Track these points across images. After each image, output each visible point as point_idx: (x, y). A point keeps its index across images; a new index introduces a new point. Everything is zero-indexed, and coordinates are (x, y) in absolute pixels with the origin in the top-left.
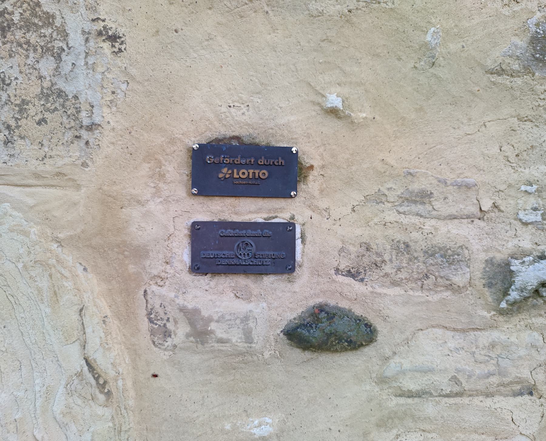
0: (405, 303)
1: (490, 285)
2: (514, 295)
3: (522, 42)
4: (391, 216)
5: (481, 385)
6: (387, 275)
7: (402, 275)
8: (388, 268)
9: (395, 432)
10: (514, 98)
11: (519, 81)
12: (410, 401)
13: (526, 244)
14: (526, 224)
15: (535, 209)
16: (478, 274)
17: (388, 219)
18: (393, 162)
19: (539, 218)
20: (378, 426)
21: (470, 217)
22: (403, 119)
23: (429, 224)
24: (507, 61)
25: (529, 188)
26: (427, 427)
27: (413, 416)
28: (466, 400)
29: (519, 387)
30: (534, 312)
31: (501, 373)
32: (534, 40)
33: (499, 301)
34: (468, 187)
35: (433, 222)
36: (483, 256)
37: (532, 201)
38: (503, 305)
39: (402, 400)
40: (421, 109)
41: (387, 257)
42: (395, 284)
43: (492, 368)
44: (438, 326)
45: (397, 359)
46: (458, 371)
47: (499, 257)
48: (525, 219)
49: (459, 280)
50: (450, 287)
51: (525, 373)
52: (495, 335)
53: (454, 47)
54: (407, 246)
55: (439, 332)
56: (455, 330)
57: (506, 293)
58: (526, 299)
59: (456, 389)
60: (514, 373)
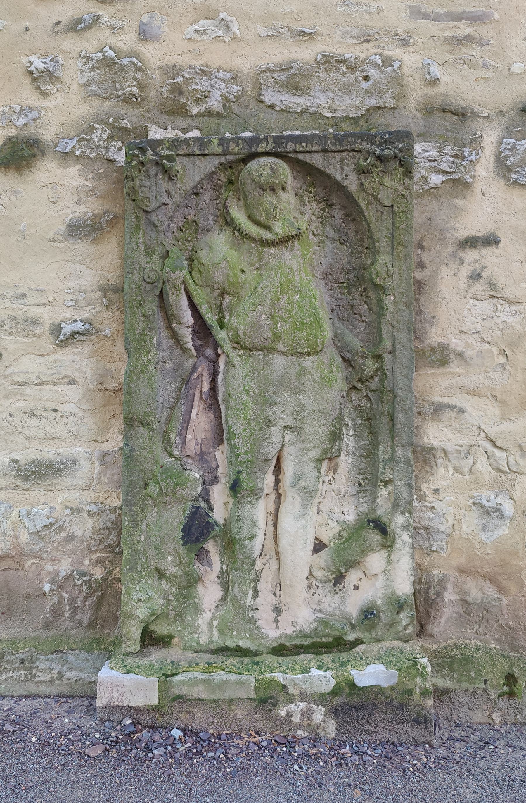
0: (15, 343)
1: (52, 334)
2: (61, 337)
3: (63, 228)
4: (8, 305)
5: (50, 379)
6: (6, 330)
7: (13, 330)
8: (6, 327)
9: (11, 400)
10: (62, 252)
11: (63, 245)
12: (20, 387)
13: (68, 316)
14: (68, 307)
15: (72, 300)
16: (47, 329)
17: (7, 306)
18: (9, 281)
19: (74, 304)
20: (4, 398)
21: (44, 305)
22: (14, 262)
23: (25, 308)
24: (56, 236)
25: (68, 291)
26: (27, 399)
27: (21, 394)
28: (45, 387)
29: (68, 380)
30: (74, 346)
31: (59, 373)
32: (69, 226)
33: (56, 340)
34: (42, 291)
35: (28, 307)
36: (49, 321)
37: (70, 297)
38: (57, 342)
39: (16, 387)
40: (21, 258)
41: (6, 322)
42: (10, 334)
43: (55, 371)
44: (32, 353)
45: (12, 368)
46: (40, 373)
47: (57, 322)
48: (67, 305)
49: (38, 332)
50: (35, 335)
51: (69, 373)
52: (56, 356)
53: (32, 231)
54: (15, 317)
55: (32, 356)
56: (39, 355)
57: (58, 337)
58: (68, 339)
59: (39, 381)
60: (64, 373)
